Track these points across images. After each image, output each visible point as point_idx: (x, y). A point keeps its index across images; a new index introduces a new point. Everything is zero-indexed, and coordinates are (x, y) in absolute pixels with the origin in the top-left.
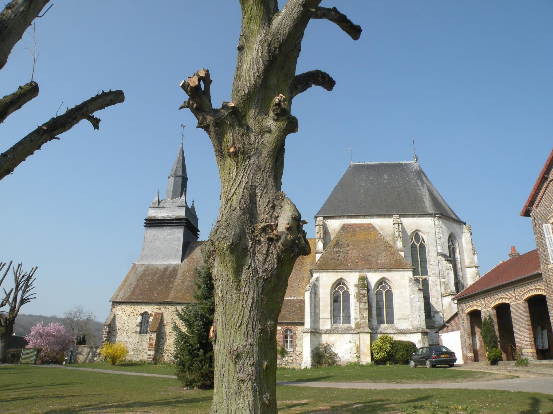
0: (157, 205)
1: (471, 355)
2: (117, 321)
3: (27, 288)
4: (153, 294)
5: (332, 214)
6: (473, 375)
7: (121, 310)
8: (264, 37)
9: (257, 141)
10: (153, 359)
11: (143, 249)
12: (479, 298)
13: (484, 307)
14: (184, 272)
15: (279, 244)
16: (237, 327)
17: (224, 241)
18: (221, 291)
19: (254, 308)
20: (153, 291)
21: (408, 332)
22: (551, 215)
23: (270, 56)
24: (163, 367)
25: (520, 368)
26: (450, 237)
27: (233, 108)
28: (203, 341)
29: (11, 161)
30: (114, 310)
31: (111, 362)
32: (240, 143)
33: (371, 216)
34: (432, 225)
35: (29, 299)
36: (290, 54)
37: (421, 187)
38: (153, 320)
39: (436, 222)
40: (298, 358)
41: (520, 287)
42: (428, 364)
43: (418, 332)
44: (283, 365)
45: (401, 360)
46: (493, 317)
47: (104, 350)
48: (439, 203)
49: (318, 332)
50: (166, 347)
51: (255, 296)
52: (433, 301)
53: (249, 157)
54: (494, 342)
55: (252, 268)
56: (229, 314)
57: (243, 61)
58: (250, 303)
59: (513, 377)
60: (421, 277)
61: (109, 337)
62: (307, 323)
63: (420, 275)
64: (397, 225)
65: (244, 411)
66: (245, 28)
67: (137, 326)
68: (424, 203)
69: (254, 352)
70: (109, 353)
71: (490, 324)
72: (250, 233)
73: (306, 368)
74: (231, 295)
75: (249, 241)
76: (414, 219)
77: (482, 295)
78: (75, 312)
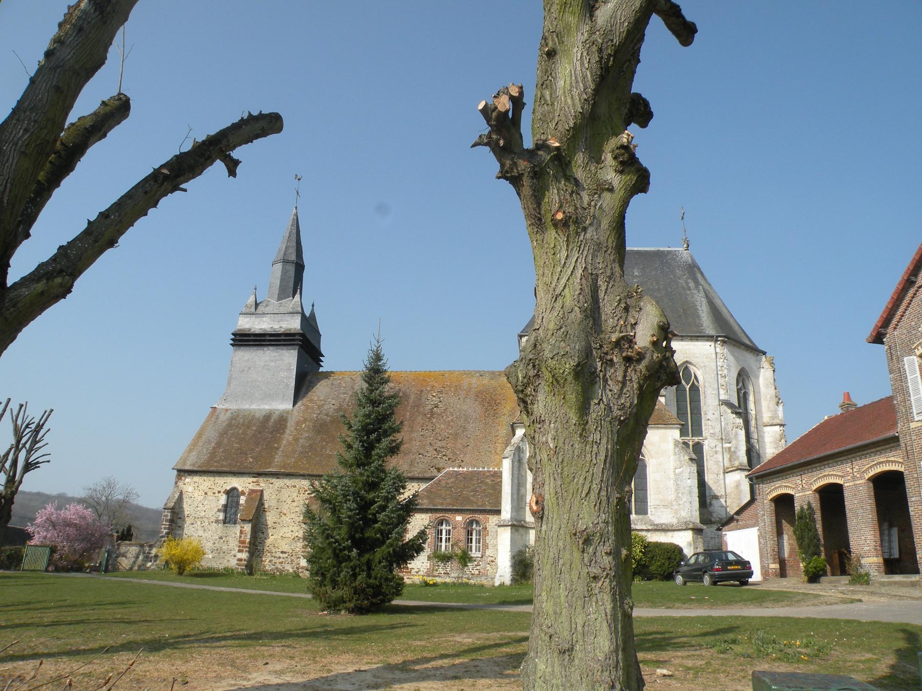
0: (253, 310)
1: (775, 566)
2: (185, 503)
3: (35, 445)
4: (246, 459)
6: (788, 597)
7: (192, 484)
8: (589, 37)
9: (593, 203)
10: (246, 566)
11: (229, 383)
12: (791, 475)
13: (799, 489)
14: (298, 423)
15: (642, 366)
16: (584, 495)
17: (565, 359)
18: (555, 438)
19: (608, 465)
20: (246, 454)
21: (670, 528)
22: (918, 343)
23: (602, 68)
24: (264, 579)
25: (858, 588)
26: (739, 375)
27: (557, 148)
28: (357, 536)
29: (116, 226)
30: (180, 484)
31: (177, 570)
32: (569, 206)
34: (712, 354)
35: (38, 463)
36: (625, 67)
38: (246, 501)
39: (718, 350)
40: (489, 567)
41: (861, 459)
42: (707, 579)
43: (687, 529)
44: (464, 579)
45: (659, 574)
46: (814, 505)
47: (164, 550)
48: (723, 317)
49: (523, 526)
50: (268, 546)
51: (609, 447)
52: (709, 479)
53: (585, 229)
54: (814, 547)
55: (603, 402)
56: (568, 475)
57: (555, 73)
58: (603, 458)
59: (852, 601)
60: (691, 440)
61: (172, 529)
62: (506, 510)
63: (690, 436)
65: (599, 625)
66: (557, 20)
67: (219, 510)
68: (699, 317)
69: (610, 533)
70: (174, 555)
71: (810, 517)
72: (599, 349)
73: (502, 585)
74: (572, 446)
75: (597, 360)
76: (682, 343)
77: (797, 470)
78: (104, 488)
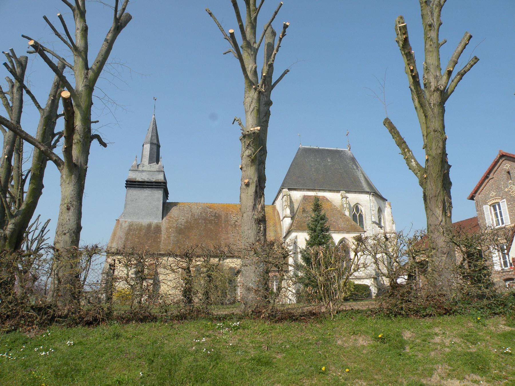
5: (294, 187)
14: (167, 229)
30: (109, 260)
33: (324, 190)
34: (368, 200)
37: (356, 171)
39: (371, 198)
64: (345, 199)
68: (361, 183)
